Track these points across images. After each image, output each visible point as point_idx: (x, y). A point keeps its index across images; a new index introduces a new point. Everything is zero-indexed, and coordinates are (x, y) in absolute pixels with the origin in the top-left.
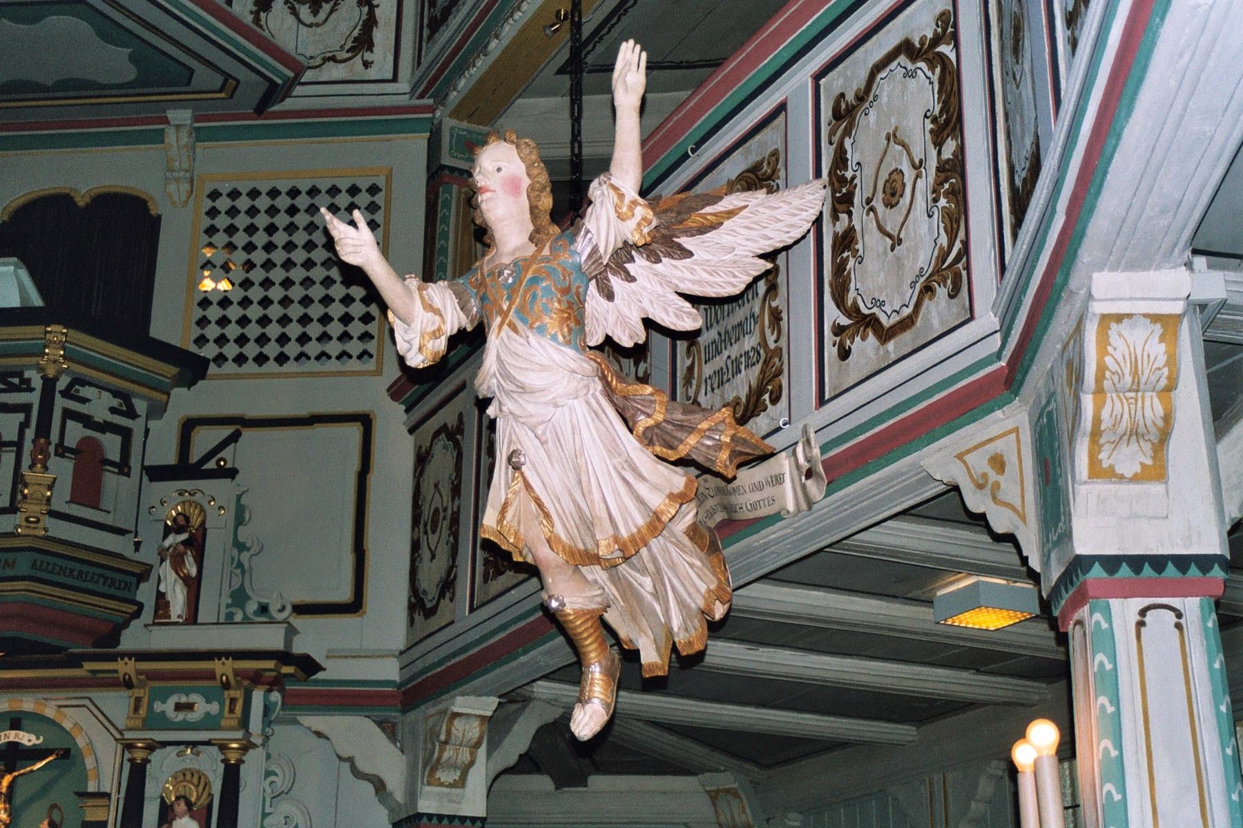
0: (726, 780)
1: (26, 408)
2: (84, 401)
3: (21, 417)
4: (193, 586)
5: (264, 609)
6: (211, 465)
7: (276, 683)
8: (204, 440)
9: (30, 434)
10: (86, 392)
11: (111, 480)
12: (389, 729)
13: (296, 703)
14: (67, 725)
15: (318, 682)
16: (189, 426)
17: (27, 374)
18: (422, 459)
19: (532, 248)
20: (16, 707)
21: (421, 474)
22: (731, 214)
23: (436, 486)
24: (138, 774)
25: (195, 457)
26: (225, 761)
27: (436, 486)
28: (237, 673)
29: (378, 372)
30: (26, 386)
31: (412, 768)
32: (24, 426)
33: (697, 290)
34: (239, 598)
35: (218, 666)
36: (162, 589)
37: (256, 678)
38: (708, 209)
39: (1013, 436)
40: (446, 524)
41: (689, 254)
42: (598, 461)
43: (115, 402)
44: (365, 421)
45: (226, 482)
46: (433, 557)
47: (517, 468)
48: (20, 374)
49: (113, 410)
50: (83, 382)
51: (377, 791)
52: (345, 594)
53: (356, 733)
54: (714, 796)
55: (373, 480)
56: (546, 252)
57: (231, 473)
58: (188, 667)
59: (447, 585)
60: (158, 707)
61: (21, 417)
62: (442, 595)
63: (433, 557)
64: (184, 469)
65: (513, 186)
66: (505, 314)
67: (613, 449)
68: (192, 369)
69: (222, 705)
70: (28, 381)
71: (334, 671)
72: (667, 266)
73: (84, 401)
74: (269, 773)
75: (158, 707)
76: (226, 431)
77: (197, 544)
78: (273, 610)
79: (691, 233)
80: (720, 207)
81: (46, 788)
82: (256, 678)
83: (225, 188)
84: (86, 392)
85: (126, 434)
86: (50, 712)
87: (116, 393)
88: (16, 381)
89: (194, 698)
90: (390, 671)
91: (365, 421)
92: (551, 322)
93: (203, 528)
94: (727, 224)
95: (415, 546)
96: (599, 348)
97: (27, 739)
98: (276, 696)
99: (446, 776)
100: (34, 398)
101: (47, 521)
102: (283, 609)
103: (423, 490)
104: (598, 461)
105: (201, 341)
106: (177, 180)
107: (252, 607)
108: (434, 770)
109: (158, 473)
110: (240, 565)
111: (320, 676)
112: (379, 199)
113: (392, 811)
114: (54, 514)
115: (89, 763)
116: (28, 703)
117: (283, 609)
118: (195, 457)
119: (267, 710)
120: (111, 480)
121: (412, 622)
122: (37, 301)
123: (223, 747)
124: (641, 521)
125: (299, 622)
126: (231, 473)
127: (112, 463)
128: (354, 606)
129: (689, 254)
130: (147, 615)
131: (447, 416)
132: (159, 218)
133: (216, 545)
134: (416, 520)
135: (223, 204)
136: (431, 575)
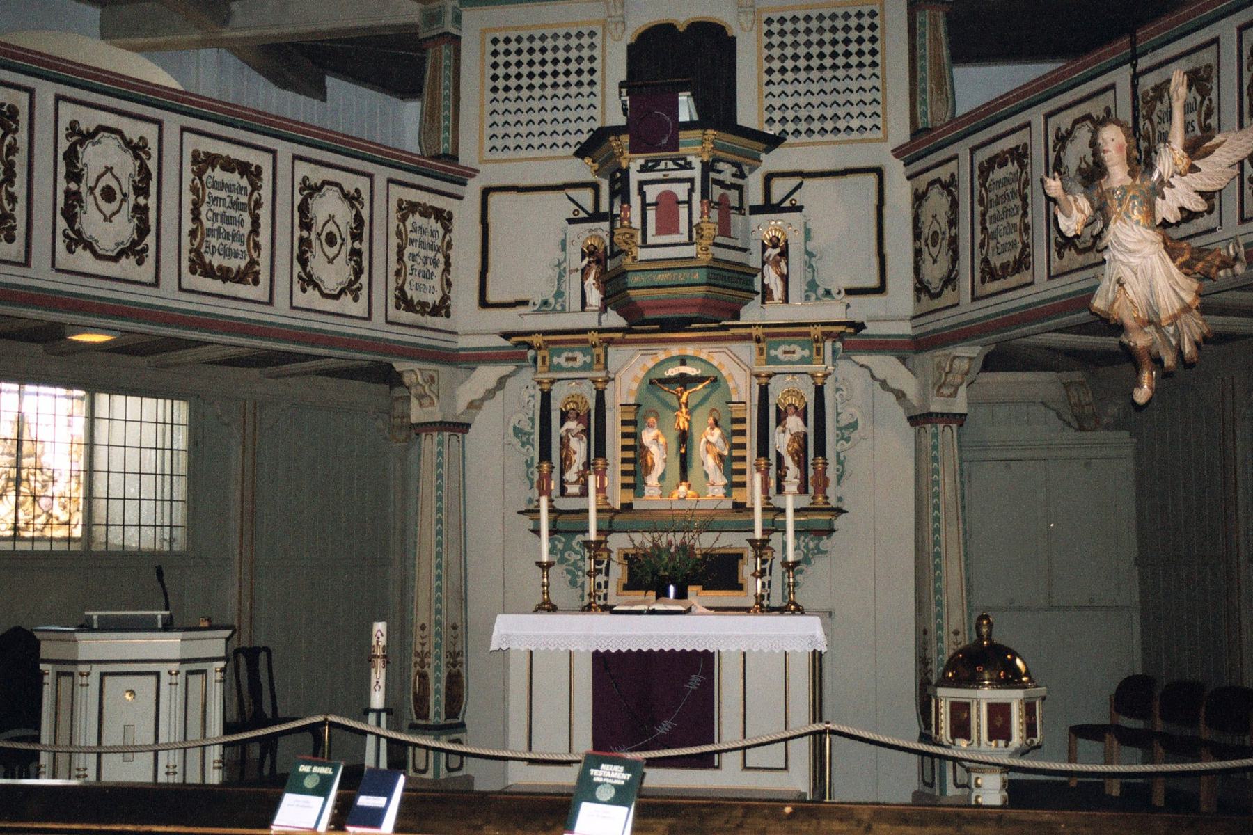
0: (1077, 376)
1: (691, 180)
2: (720, 172)
3: (688, 185)
4: (785, 279)
5: (828, 293)
6: (787, 204)
7: (839, 336)
8: (780, 188)
9: (697, 197)
10: (721, 166)
11: (736, 219)
12: (903, 360)
13: (851, 349)
14: (715, 363)
15: (864, 336)
16: (769, 178)
17: (689, 159)
18: (919, 198)
19: (1130, 180)
20: (683, 353)
21: (919, 206)
22: (1218, 145)
23: (934, 217)
24: (764, 391)
25: (775, 199)
26: (815, 384)
27: (934, 217)
28: (823, 333)
29: (885, 139)
30: (688, 166)
31: (923, 387)
32: (691, 191)
33: (1203, 189)
34: (812, 286)
35: (812, 329)
36: (766, 281)
37: (828, 335)
38: (1208, 144)
39: (1214, 47)
40: (945, 243)
41: (1200, 170)
42: (1162, 283)
43: (734, 170)
44: (879, 172)
45: (796, 215)
46: (935, 261)
47: (1121, 285)
48: (685, 159)
49: (734, 175)
50: (720, 160)
51: (898, 398)
52: (874, 282)
53: (885, 365)
54: (1067, 386)
55: (887, 211)
56: (1138, 182)
57: (799, 209)
58: (795, 331)
59: (950, 280)
60: (773, 353)
61: (688, 185)
62: (945, 285)
63: (935, 261)
64: (768, 207)
65: (1120, 148)
66: (1119, 214)
67: (1170, 276)
68: (774, 142)
69: (811, 351)
70: (690, 163)
71: (871, 329)
72: (1189, 178)
73: (720, 172)
74: (838, 389)
75: (773, 353)
76: (796, 181)
77: (784, 254)
78: (834, 292)
79: (1199, 158)
80: (1214, 141)
81: (705, 399)
82: (828, 335)
83: (776, 17)
84: (721, 166)
85: (740, 188)
86: (704, 356)
87: (734, 164)
88: (682, 162)
89: (793, 347)
90: (906, 329)
91: (879, 172)
92: (1136, 215)
93: (786, 242)
94: (1217, 151)
95: (918, 253)
96: (1160, 224)
97: (690, 370)
98: (839, 345)
99: (946, 391)
100: (696, 174)
101: (712, 249)
102: (839, 292)
103: (922, 218)
104: (1162, 283)
105: (770, 121)
106: (746, 13)
107: (821, 291)
108: (940, 388)
109: (755, 210)
110: (811, 266)
111: (864, 332)
112: (877, 20)
113: (906, 409)
114: (716, 245)
115: (731, 385)
116: (690, 350)
117: (839, 292)
118: (775, 199)
119: (834, 352)
120: (736, 219)
121: (919, 299)
122: (695, 118)
123: (813, 376)
124: (1178, 306)
125: (853, 300)
126: (799, 209)
127: (733, 208)
128: (881, 289)
129: (1200, 170)
130: (759, 298)
131: (943, 173)
132: (734, 38)
133: (795, 253)
134: (917, 235)
135: (776, 27)
136: (934, 273)
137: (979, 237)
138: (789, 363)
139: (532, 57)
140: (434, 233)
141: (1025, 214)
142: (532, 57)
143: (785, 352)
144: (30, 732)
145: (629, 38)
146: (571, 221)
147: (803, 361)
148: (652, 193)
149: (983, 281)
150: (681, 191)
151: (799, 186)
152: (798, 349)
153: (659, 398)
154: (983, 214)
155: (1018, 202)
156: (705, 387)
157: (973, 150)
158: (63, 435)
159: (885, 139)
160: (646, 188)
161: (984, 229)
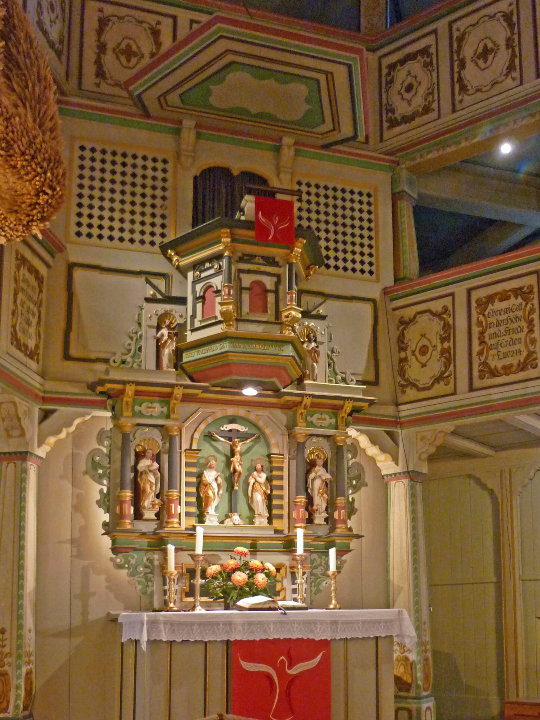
6: (314, 313)
126: (323, 318)
137: (476, 348)
138: (321, 427)
139: (129, 166)
140: (33, 289)
141: (531, 331)
142: (129, 166)
143: (325, 420)
144: (207, 541)
145: (195, 171)
146: (147, 300)
147: (329, 427)
148: (247, 280)
149: (481, 377)
150: (269, 282)
151: (324, 301)
152: (327, 417)
153: (212, 445)
154: (482, 333)
155: (523, 324)
156: (252, 441)
157: (469, 291)
158: (407, 256)
159: (378, 280)
160: (242, 275)
161: (482, 342)
